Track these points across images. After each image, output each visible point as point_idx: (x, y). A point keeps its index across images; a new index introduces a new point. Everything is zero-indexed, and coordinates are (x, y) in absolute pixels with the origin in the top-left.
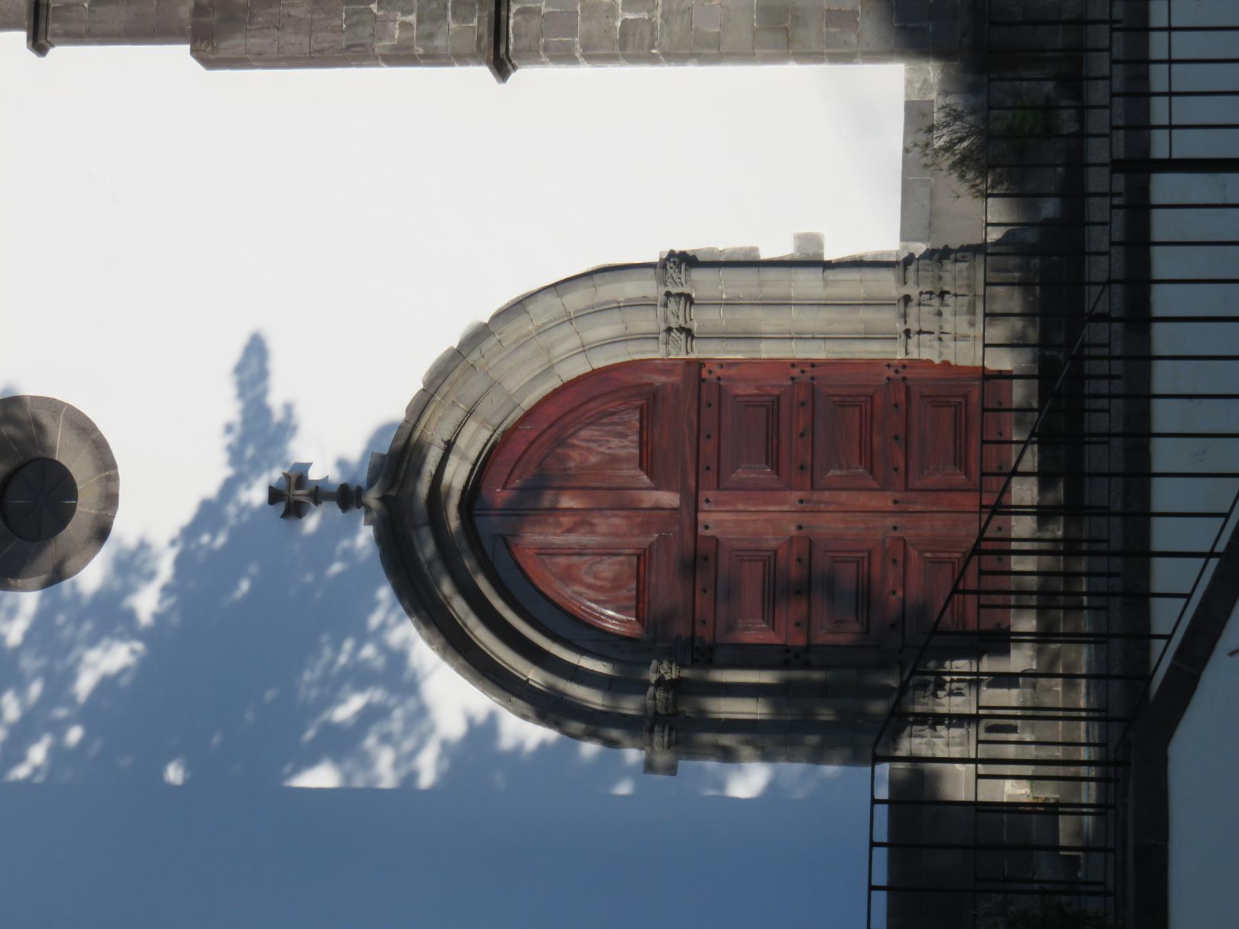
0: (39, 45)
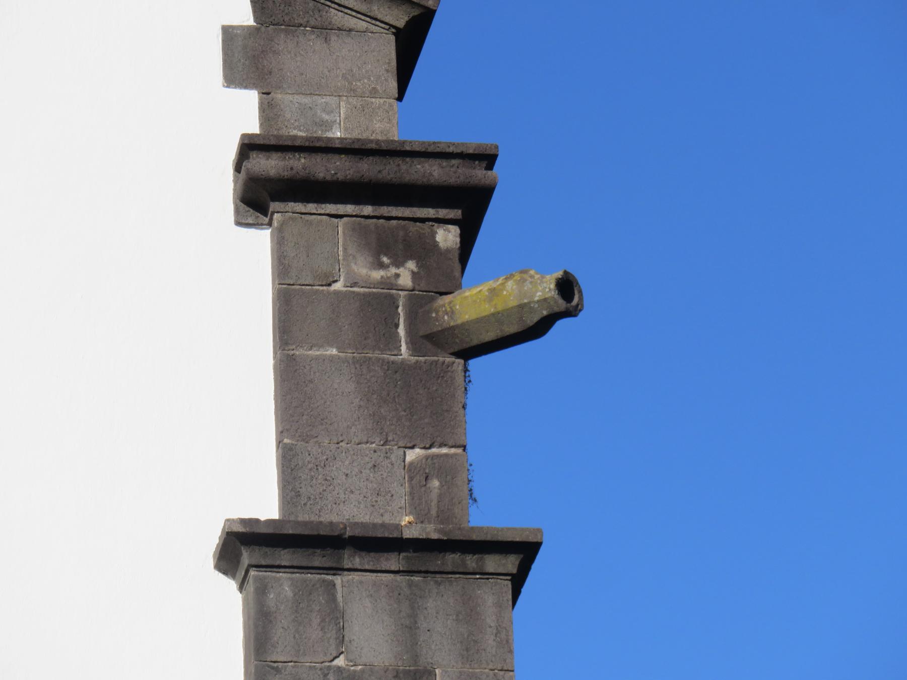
0: (244, 548)
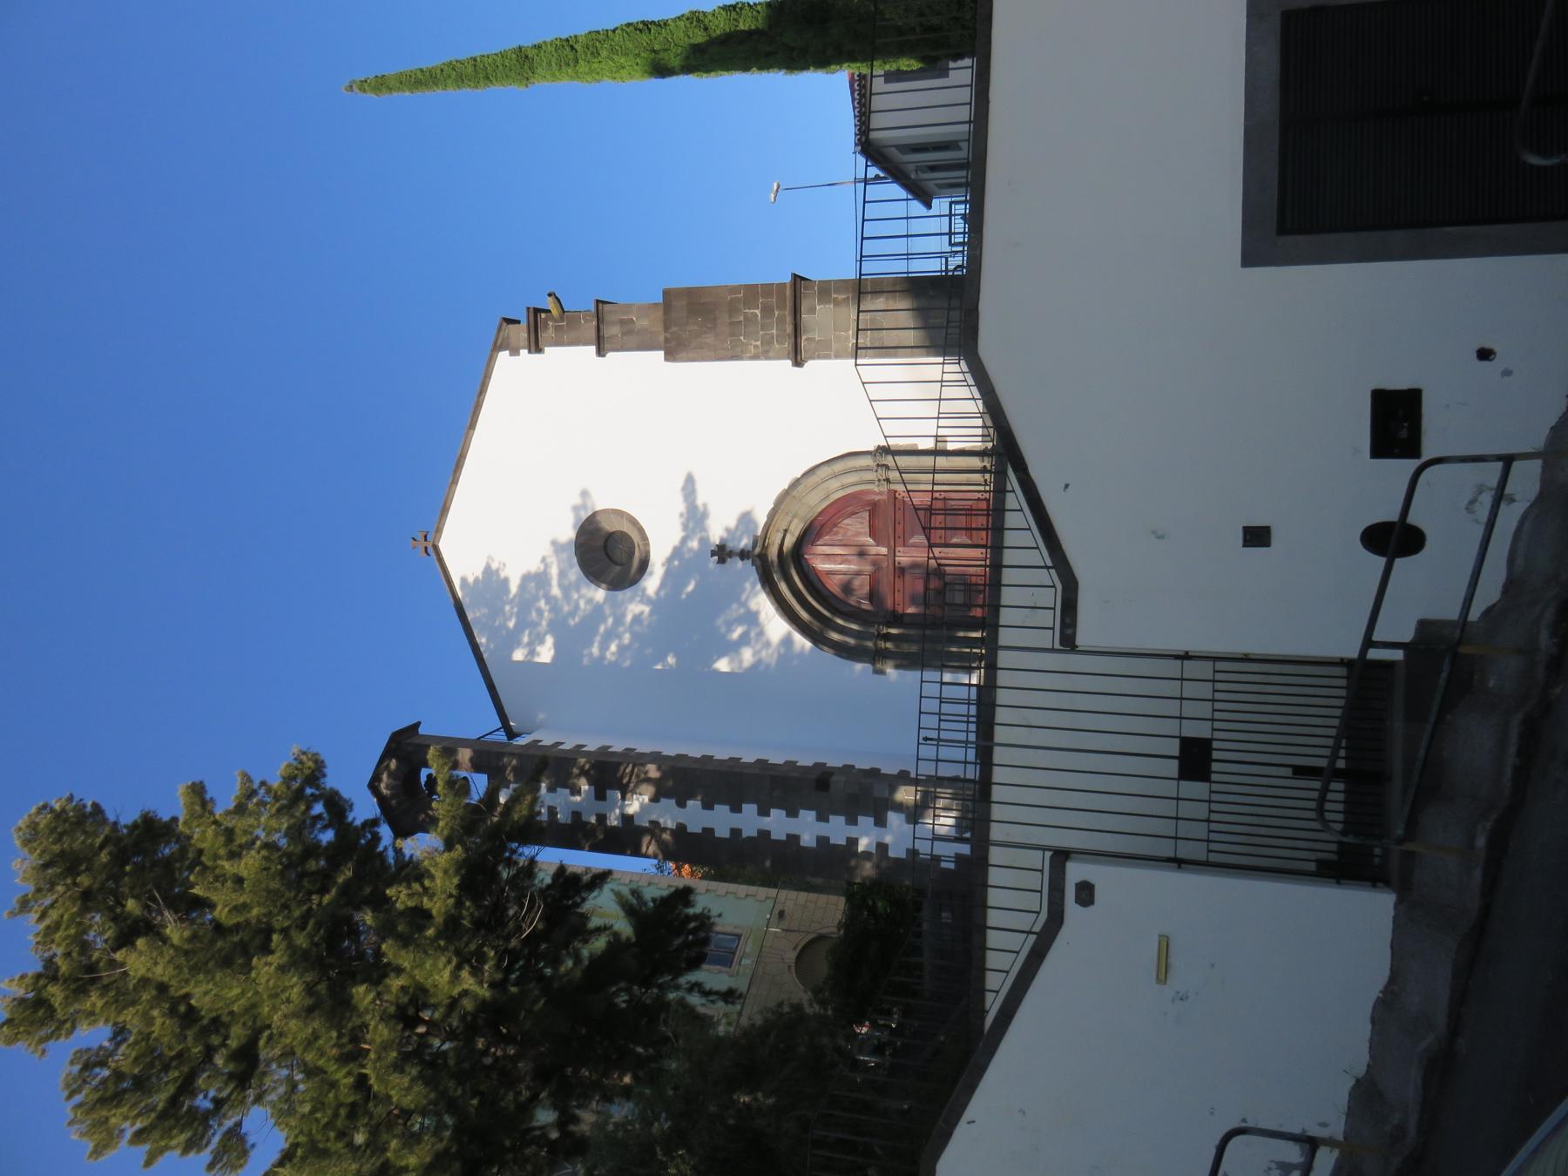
0: (600, 352)
